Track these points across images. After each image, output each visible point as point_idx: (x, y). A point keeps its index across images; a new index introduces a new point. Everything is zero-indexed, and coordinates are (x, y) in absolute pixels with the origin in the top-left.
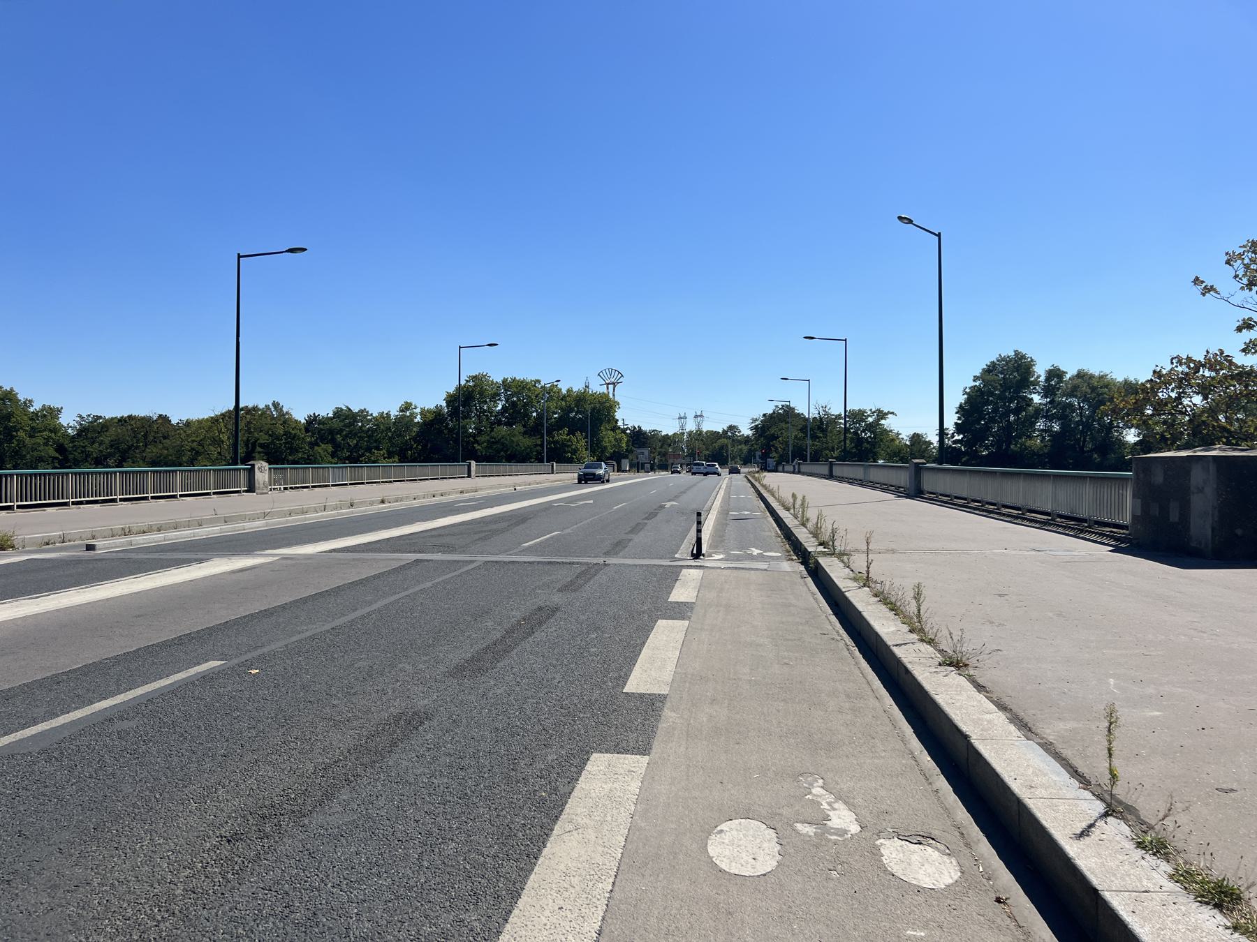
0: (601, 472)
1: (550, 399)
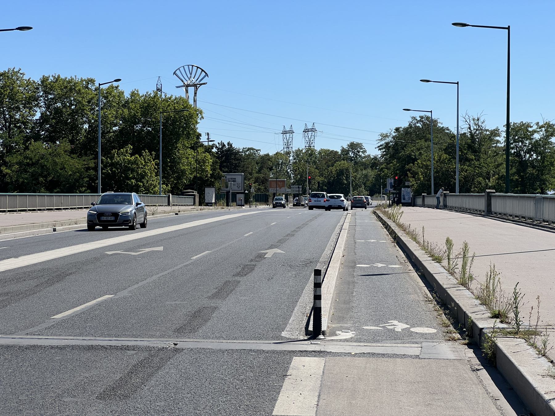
0: (129, 209)
1: (108, 105)
